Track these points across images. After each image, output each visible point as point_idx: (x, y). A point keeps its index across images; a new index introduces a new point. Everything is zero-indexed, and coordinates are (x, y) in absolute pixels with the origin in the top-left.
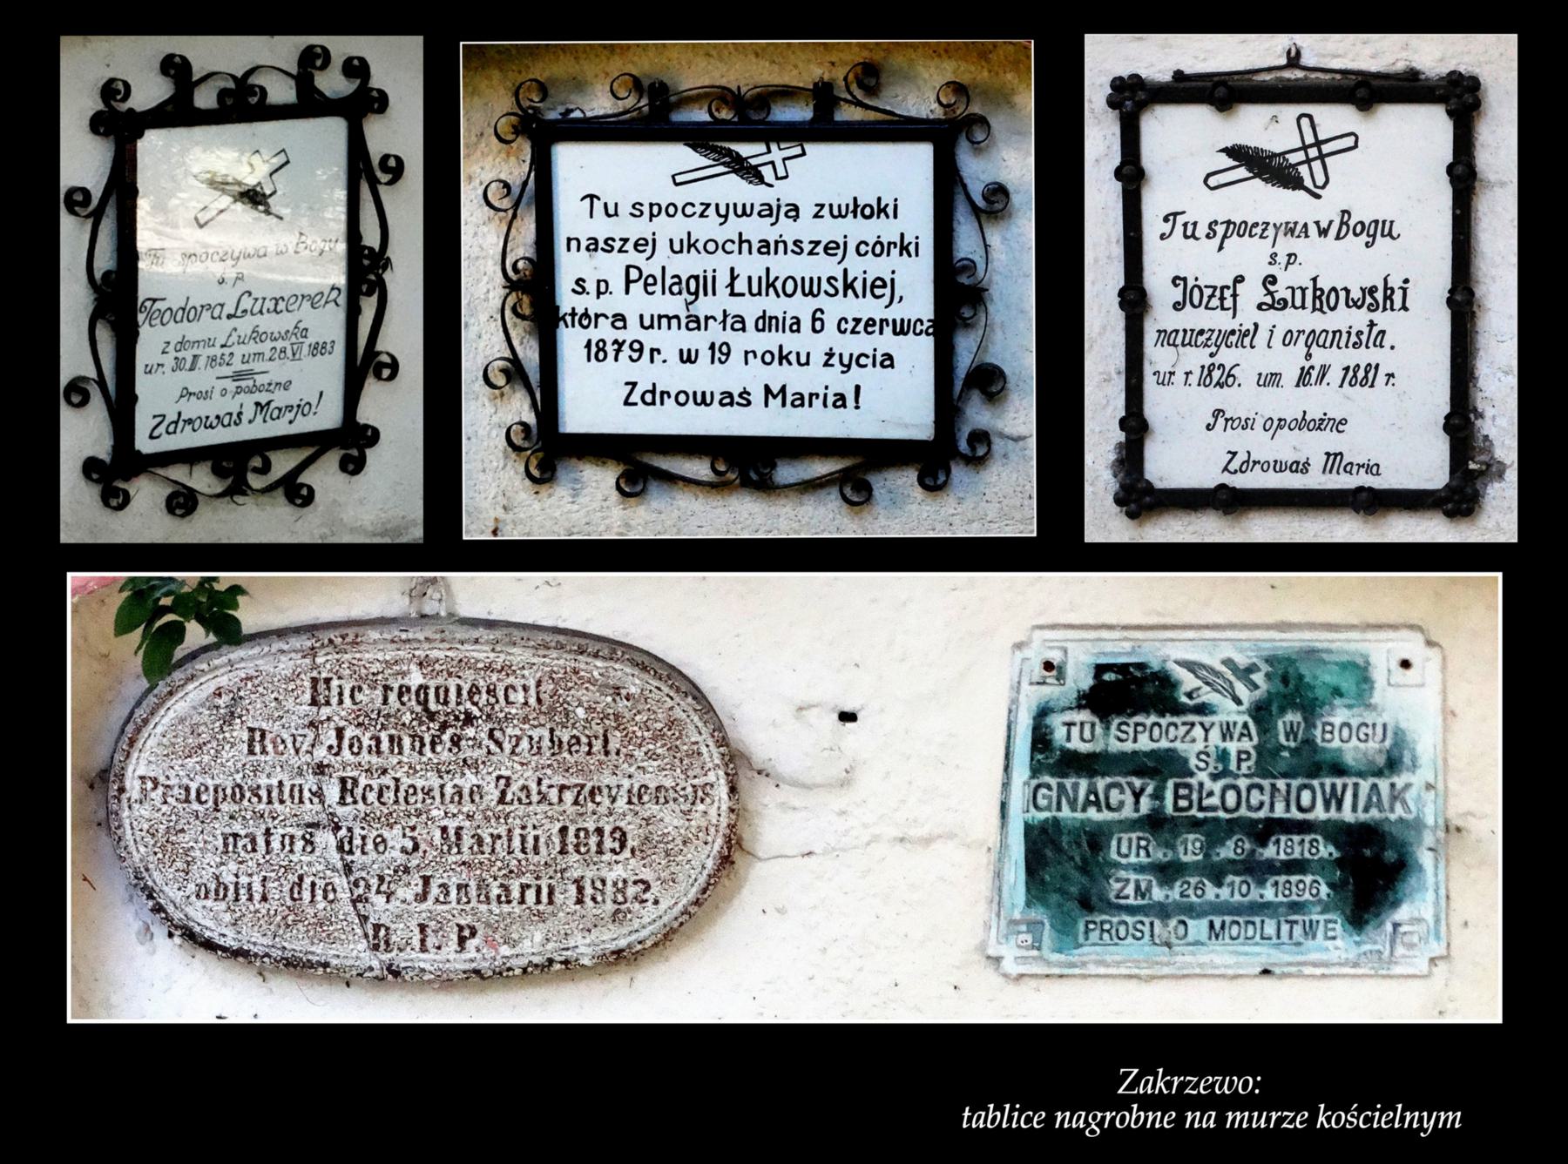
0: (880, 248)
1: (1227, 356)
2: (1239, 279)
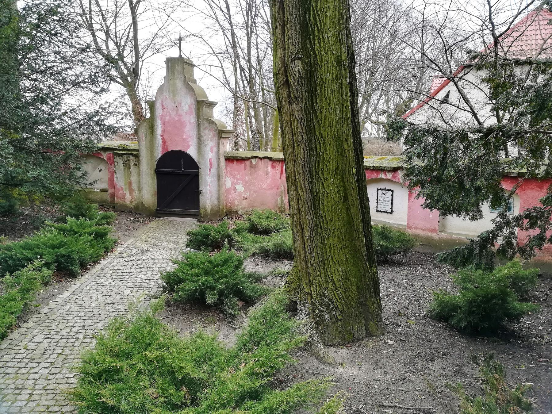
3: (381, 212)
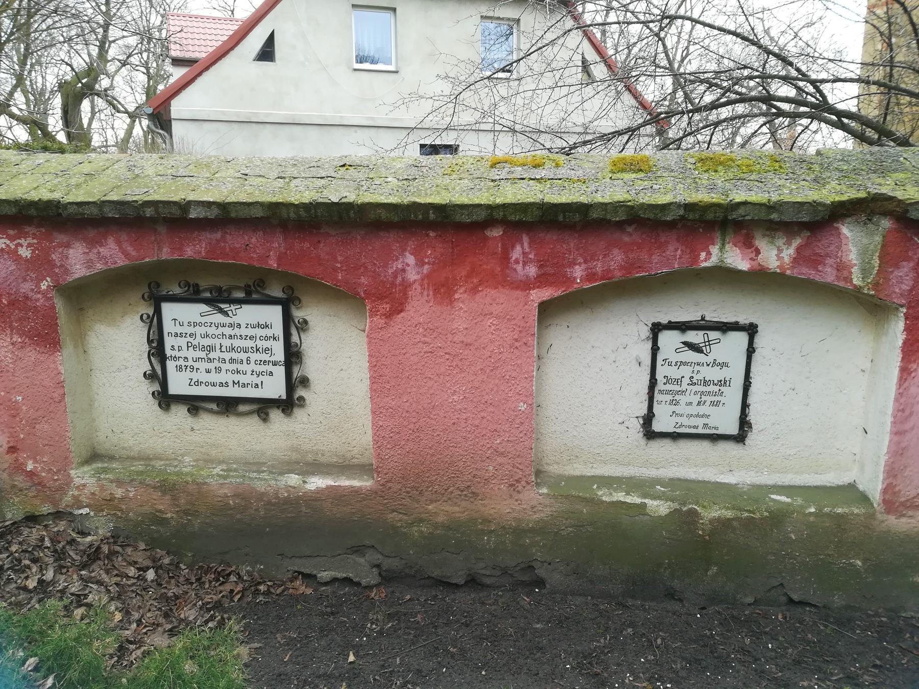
0: (267, 338)
1: (677, 397)
2: (683, 377)
3: (675, 436)
